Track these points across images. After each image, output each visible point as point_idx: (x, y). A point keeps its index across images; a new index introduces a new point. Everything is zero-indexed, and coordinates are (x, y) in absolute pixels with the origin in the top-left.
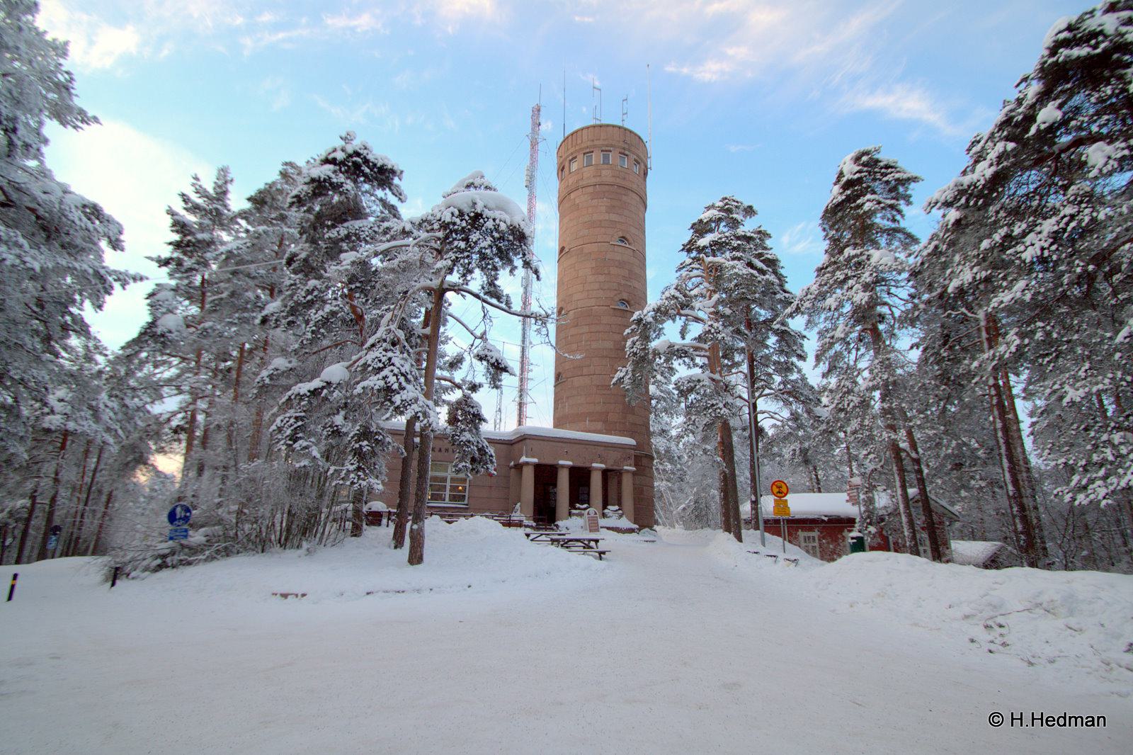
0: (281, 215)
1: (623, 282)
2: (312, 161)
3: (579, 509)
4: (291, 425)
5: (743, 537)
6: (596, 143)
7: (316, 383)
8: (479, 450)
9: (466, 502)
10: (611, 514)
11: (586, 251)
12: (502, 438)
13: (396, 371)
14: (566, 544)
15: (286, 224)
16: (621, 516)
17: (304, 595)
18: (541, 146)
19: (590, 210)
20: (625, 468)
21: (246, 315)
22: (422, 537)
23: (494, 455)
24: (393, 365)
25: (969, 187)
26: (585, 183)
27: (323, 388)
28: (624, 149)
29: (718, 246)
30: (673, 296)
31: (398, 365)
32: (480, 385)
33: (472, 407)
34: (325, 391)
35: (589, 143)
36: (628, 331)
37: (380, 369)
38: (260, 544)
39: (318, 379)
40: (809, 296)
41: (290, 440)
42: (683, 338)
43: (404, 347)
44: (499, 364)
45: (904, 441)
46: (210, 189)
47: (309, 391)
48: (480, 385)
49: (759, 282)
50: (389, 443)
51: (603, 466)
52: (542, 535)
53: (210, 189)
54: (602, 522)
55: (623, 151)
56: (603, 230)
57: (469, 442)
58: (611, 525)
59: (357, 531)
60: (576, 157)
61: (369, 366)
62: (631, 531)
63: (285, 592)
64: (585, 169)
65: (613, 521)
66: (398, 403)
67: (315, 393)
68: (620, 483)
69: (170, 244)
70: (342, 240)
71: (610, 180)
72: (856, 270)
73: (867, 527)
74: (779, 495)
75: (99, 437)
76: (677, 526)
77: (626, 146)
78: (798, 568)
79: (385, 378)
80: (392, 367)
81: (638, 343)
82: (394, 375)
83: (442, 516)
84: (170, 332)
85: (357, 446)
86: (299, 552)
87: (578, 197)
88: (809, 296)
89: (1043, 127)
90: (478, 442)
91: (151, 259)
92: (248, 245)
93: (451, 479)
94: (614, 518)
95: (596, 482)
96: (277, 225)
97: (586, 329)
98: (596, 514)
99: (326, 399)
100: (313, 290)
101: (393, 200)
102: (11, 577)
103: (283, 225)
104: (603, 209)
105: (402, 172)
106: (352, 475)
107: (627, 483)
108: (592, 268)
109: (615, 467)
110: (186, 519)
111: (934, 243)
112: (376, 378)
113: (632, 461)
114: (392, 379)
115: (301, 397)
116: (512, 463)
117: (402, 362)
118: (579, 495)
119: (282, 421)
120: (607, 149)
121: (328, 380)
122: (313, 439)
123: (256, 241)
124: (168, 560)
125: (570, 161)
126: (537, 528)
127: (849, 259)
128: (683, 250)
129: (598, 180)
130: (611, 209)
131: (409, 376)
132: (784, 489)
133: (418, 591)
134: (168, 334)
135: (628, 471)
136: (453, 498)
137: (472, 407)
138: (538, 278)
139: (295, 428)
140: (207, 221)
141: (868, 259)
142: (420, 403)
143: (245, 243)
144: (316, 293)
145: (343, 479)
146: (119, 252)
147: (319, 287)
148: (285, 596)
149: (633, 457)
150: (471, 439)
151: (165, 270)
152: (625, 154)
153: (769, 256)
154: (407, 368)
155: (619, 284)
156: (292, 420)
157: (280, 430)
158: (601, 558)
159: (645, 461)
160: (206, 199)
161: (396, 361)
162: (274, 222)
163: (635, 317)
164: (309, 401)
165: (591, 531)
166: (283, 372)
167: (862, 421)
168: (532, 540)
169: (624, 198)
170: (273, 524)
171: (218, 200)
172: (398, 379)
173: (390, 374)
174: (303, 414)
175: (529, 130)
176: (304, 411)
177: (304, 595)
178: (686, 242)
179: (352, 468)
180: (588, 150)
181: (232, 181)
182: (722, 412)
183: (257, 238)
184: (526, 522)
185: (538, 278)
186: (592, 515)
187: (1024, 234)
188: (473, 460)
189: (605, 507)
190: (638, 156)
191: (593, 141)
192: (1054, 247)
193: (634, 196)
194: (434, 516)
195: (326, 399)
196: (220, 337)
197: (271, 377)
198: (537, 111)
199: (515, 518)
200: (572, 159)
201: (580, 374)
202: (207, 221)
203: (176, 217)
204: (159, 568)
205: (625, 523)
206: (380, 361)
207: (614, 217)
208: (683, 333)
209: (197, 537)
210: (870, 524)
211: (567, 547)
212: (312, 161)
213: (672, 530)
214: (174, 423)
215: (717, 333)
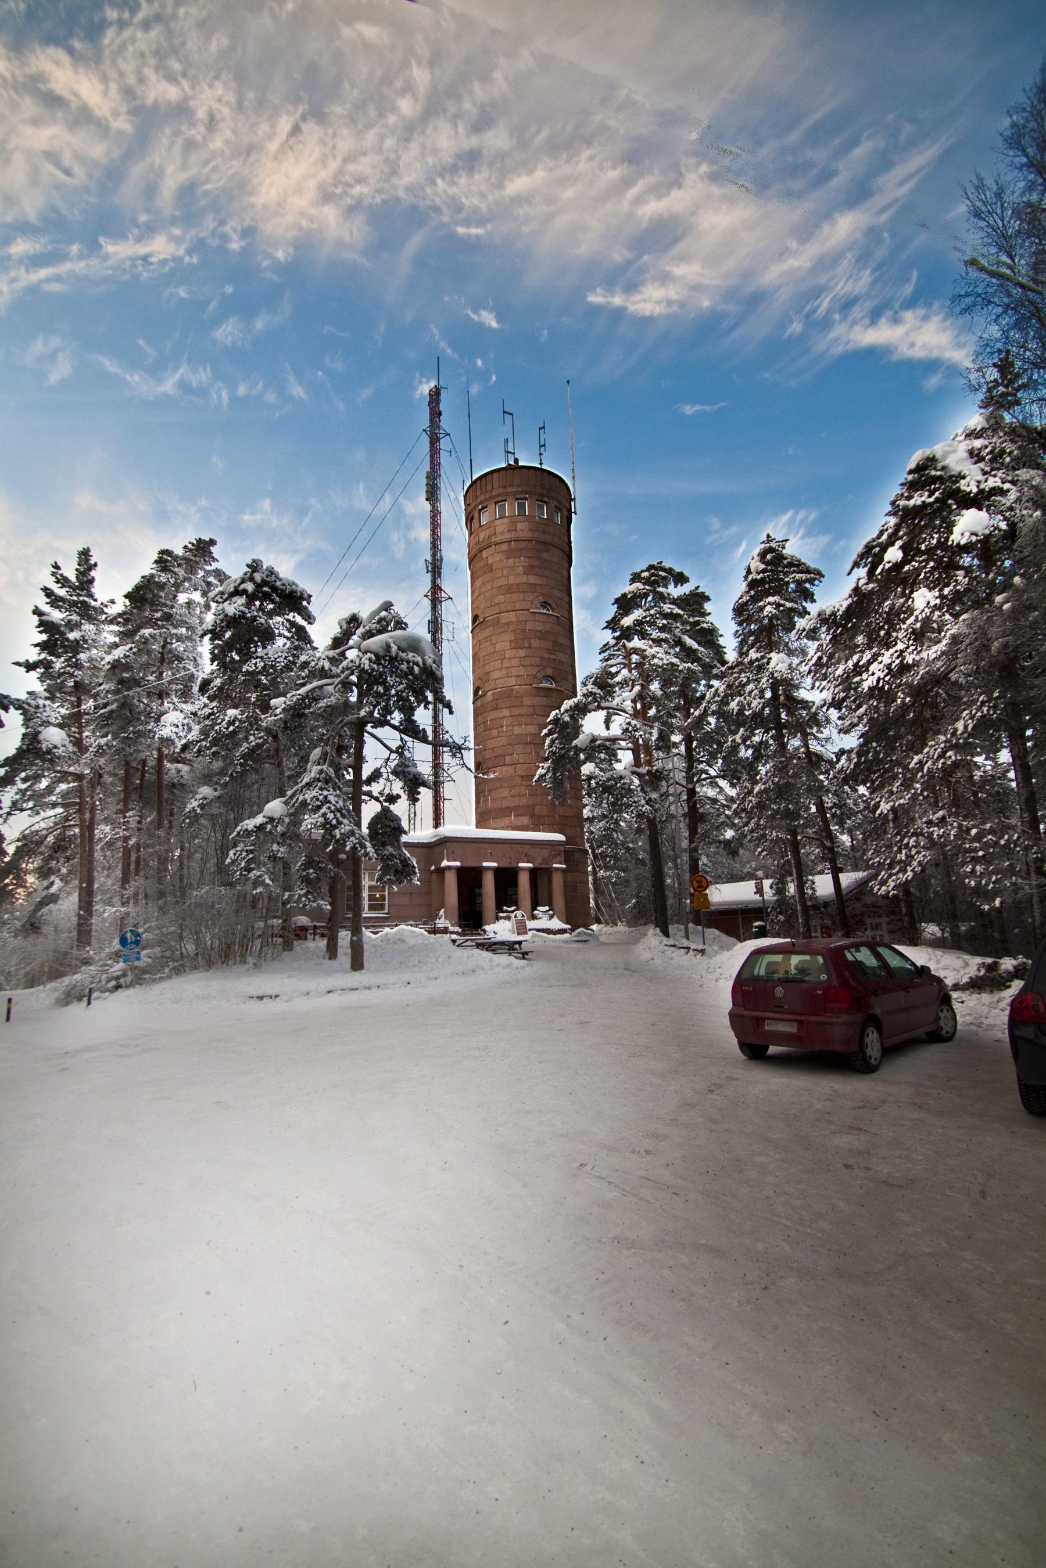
0: (166, 613)
1: (546, 656)
2: (190, 546)
3: (507, 911)
4: (244, 858)
5: (670, 932)
6: (509, 489)
7: (259, 820)
8: (401, 862)
9: (386, 911)
10: (541, 915)
11: (503, 621)
13: (333, 808)
14: (492, 947)
15: (172, 624)
16: (551, 917)
17: (277, 996)
18: (444, 444)
19: (505, 572)
20: (555, 865)
22: (362, 947)
24: (329, 802)
25: (830, 616)
26: (498, 539)
27: (267, 823)
28: (542, 495)
29: (639, 630)
30: (591, 692)
31: (334, 802)
32: (398, 796)
33: (393, 821)
35: (501, 490)
36: (545, 731)
37: (319, 807)
39: (261, 815)
40: (716, 699)
41: (245, 871)
42: (608, 728)
43: (336, 783)
44: (416, 779)
45: (835, 830)
46: (72, 577)
47: (255, 827)
48: (398, 796)
49: (681, 671)
50: (331, 870)
51: (530, 865)
52: (467, 940)
53: (72, 577)
54: (531, 924)
55: (540, 498)
56: (521, 595)
57: (392, 855)
58: (541, 927)
59: (288, 946)
60: (486, 507)
61: (309, 804)
62: (562, 931)
63: (260, 993)
64: (498, 522)
65: (543, 923)
66: (338, 836)
67: (260, 828)
68: (550, 881)
69: (36, 645)
70: (260, 673)
71: (526, 534)
72: (757, 674)
73: (777, 917)
74: (699, 889)
76: (619, 923)
77: (545, 492)
78: (704, 957)
79: (324, 815)
80: (328, 805)
81: (557, 741)
82: (332, 812)
84: (56, 747)
85: (305, 873)
86: (247, 966)
88: (716, 699)
89: (887, 566)
91: (18, 664)
92: (135, 650)
93: (369, 887)
94: (546, 920)
95: (524, 880)
96: (163, 627)
97: (506, 712)
98: (523, 916)
100: (234, 721)
101: (299, 620)
102: (6, 1002)
103: (170, 627)
104: (521, 570)
105: (310, 596)
106: (304, 899)
107: (557, 883)
108: (511, 641)
109: (543, 866)
110: (137, 943)
111: (819, 654)
112: (317, 816)
113: (562, 859)
114: (331, 816)
115: (248, 833)
116: (433, 868)
117: (336, 799)
118: (506, 897)
119: (235, 854)
120: (522, 496)
121: (270, 815)
122: (263, 869)
123: (142, 647)
124: (122, 980)
125: (480, 511)
127: (751, 662)
128: (606, 627)
129: (513, 535)
131: (344, 811)
132: (704, 884)
134: (55, 750)
135: (557, 869)
137: (393, 821)
138: (451, 712)
139: (248, 861)
140: (75, 617)
141: (768, 663)
143: (131, 649)
144: (237, 724)
145: (295, 902)
147: (239, 717)
148: (261, 998)
149: (563, 854)
150: (394, 853)
151: (34, 675)
152: (542, 501)
153: (705, 625)
155: (542, 658)
156: (244, 854)
158: (524, 958)
159: (578, 856)
160: (67, 589)
161: (332, 798)
162: (160, 623)
163: (551, 717)
164: (256, 836)
165: (519, 934)
166: (212, 800)
167: (759, 821)
168: (459, 946)
171: (82, 590)
172: (335, 815)
173: (327, 811)
174: (252, 848)
175: (426, 423)
176: (253, 845)
177: (277, 996)
178: (609, 618)
179: (302, 892)
180: (500, 499)
181: (96, 565)
182: (644, 809)
183: (144, 643)
184: (451, 929)
185: (451, 712)
186: (520, 917)
187: (869, 663)
188: (396, 872)
189: (534, 908)
190: (559, 502)
191: (505, 487)
192: (887, 678)
195: (270, 832)
197: (202, 806)
199: (439, 926)
200: (483, 508)
201: (501, 763)
202: (75, 617)
203: (44, 618)
204: (118, 987)
205: (556, 924)
206: (318, 799)
208: (607, 723)
209: (145, 957)
210: (780, 913)
211: (493, 950)
212: (190, 546)
213: (615, 928)
215: (635, 731)
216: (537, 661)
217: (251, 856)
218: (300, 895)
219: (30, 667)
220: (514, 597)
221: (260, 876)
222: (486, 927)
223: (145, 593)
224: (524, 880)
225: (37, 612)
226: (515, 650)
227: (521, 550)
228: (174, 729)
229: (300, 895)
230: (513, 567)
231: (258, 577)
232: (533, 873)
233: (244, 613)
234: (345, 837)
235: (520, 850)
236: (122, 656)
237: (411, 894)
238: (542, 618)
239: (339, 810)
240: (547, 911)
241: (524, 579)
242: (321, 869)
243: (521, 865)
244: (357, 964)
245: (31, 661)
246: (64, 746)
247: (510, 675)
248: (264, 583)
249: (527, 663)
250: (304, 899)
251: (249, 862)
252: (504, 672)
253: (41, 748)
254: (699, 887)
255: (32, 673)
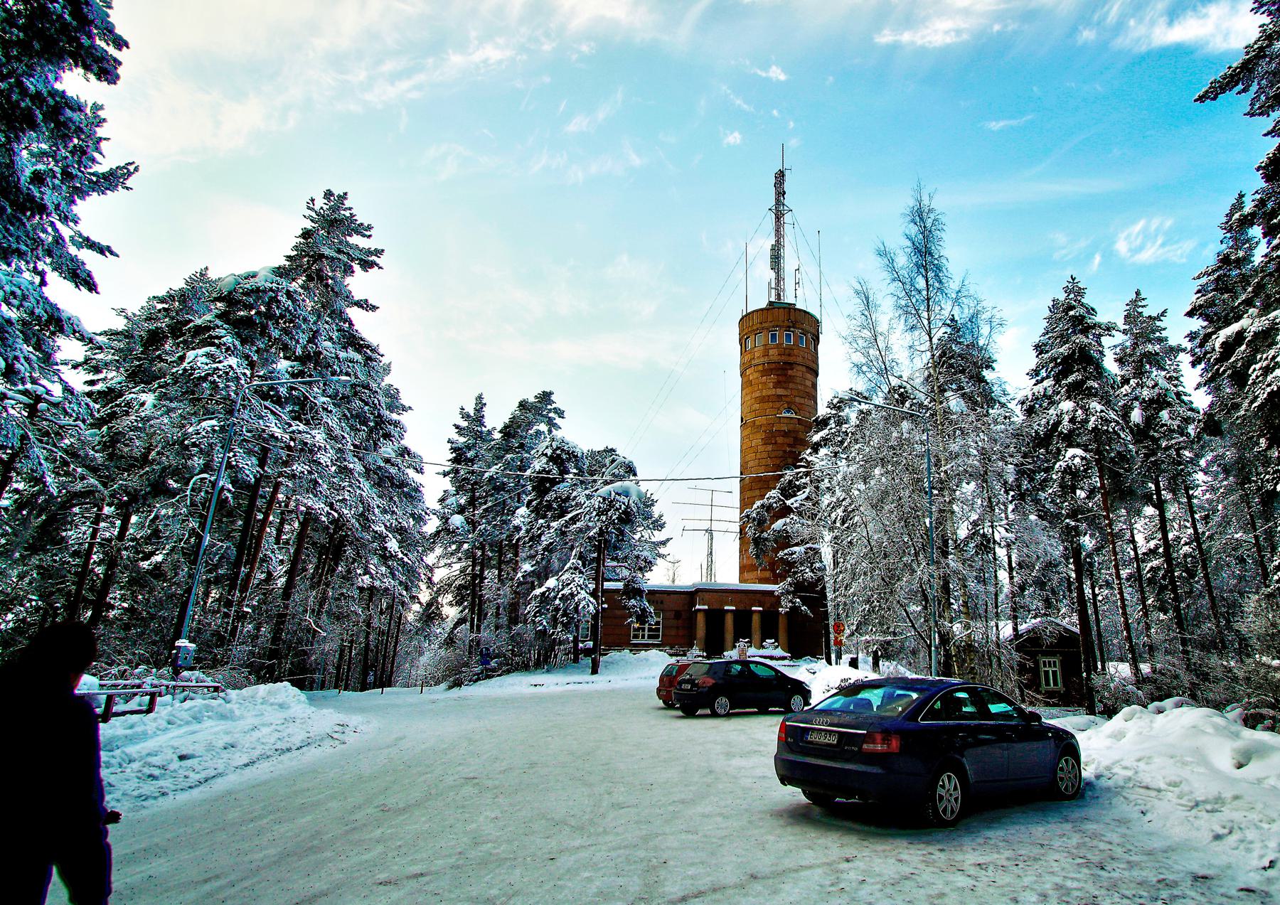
1: (788, 449)
6: (764, 325)
7: (543, 589)
11: (757, 423)
16: (777, 647)
18: (787, 218)
28: (789, 327)
37: (569, 584)
38: (525, 667)
56: (771, 404)
62: (783, 658)
67: (543, 594)
71: (776, 358)
84: (458, 528)
87: (753, 374)
96: (518, 453)
115: (536, 597)
126: (791, 658)
129: (766, 359)
130: (777, 384)
135: (755, 611)
136: (650, 637)
151: (448, 478)
169: (790, 372)
193: (800, 368)
198: (780, 176)
205: (779, 652)
207: (780, 391)
216: (781, 453)
219: (445, 474)
220: (766, 405)
222: (725, 653)
227: (772, 370)
228: (522, 519)
230: (765, 383)
238: (785, 421)
239: (580, 586)
241: (773, 392)
244: (594, 671)
248: (558, 448)
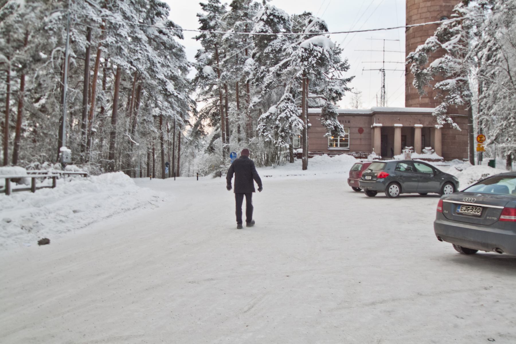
7: (267, 114)
9: (348, 147)
12: (366, 113)
16: (433, 153)
21: (238, 66)
23: (343, 128)
27: (270, 115)
34: (270, 116)
37: (285, 110)
51: (421, 126)
57: (330, 124)
63: (267, 175)
67: (268, 117)
75: (176, 117)
83: (328, 154)
84: (209, 75)
86: (271, 167)
90: (334, 124)
91: (193, 38)
95: (418, 135)
99: (271, 119)
103: (247, 19)
114: (288, 113)
115: (263, 119)
133: (301, 175)
136: (341, 145)
142: (297, 121)
146: (182, 39)
147: (265, 70)
150: (331, 123)
151: (199, 41)
154: (292, 109)
155: (441, 6)
156: (262, 126)
157: (259, 129)
161: (289, 106)
162: (243, 18)
170: (262, 158)
173: (287, 111)
189: (423, 148)
194: (325, 154)
195: (271, 119)
196: (230, 79)
197: (254, 106)
214: (212, 111)
217: (265, 127)
218: (279, 142)
219: (197, 38)
221: (268, 135)
223: (237, 4)
224: (418, 135)
225: (198, 15)
226: (425, 3)
228: (250, 67)
229: (279, 142)
231: (268, 12)
232: (423, 129)
233: (262, 29)
234: (292, 121)
235: (416, 118)
236: (229, 36)
237: (361, 139)
240: (430, 150)
242: (287, 132)
243: (416, 125)
245: (198, 36)
246: (212, 74)
247: (422, 17)
249: (432, 10)
250: (280, 143)
251: (264, 130)
252: (419, 16)
253: (203, 76)
254: (481, 140)
255: (199, 41)
